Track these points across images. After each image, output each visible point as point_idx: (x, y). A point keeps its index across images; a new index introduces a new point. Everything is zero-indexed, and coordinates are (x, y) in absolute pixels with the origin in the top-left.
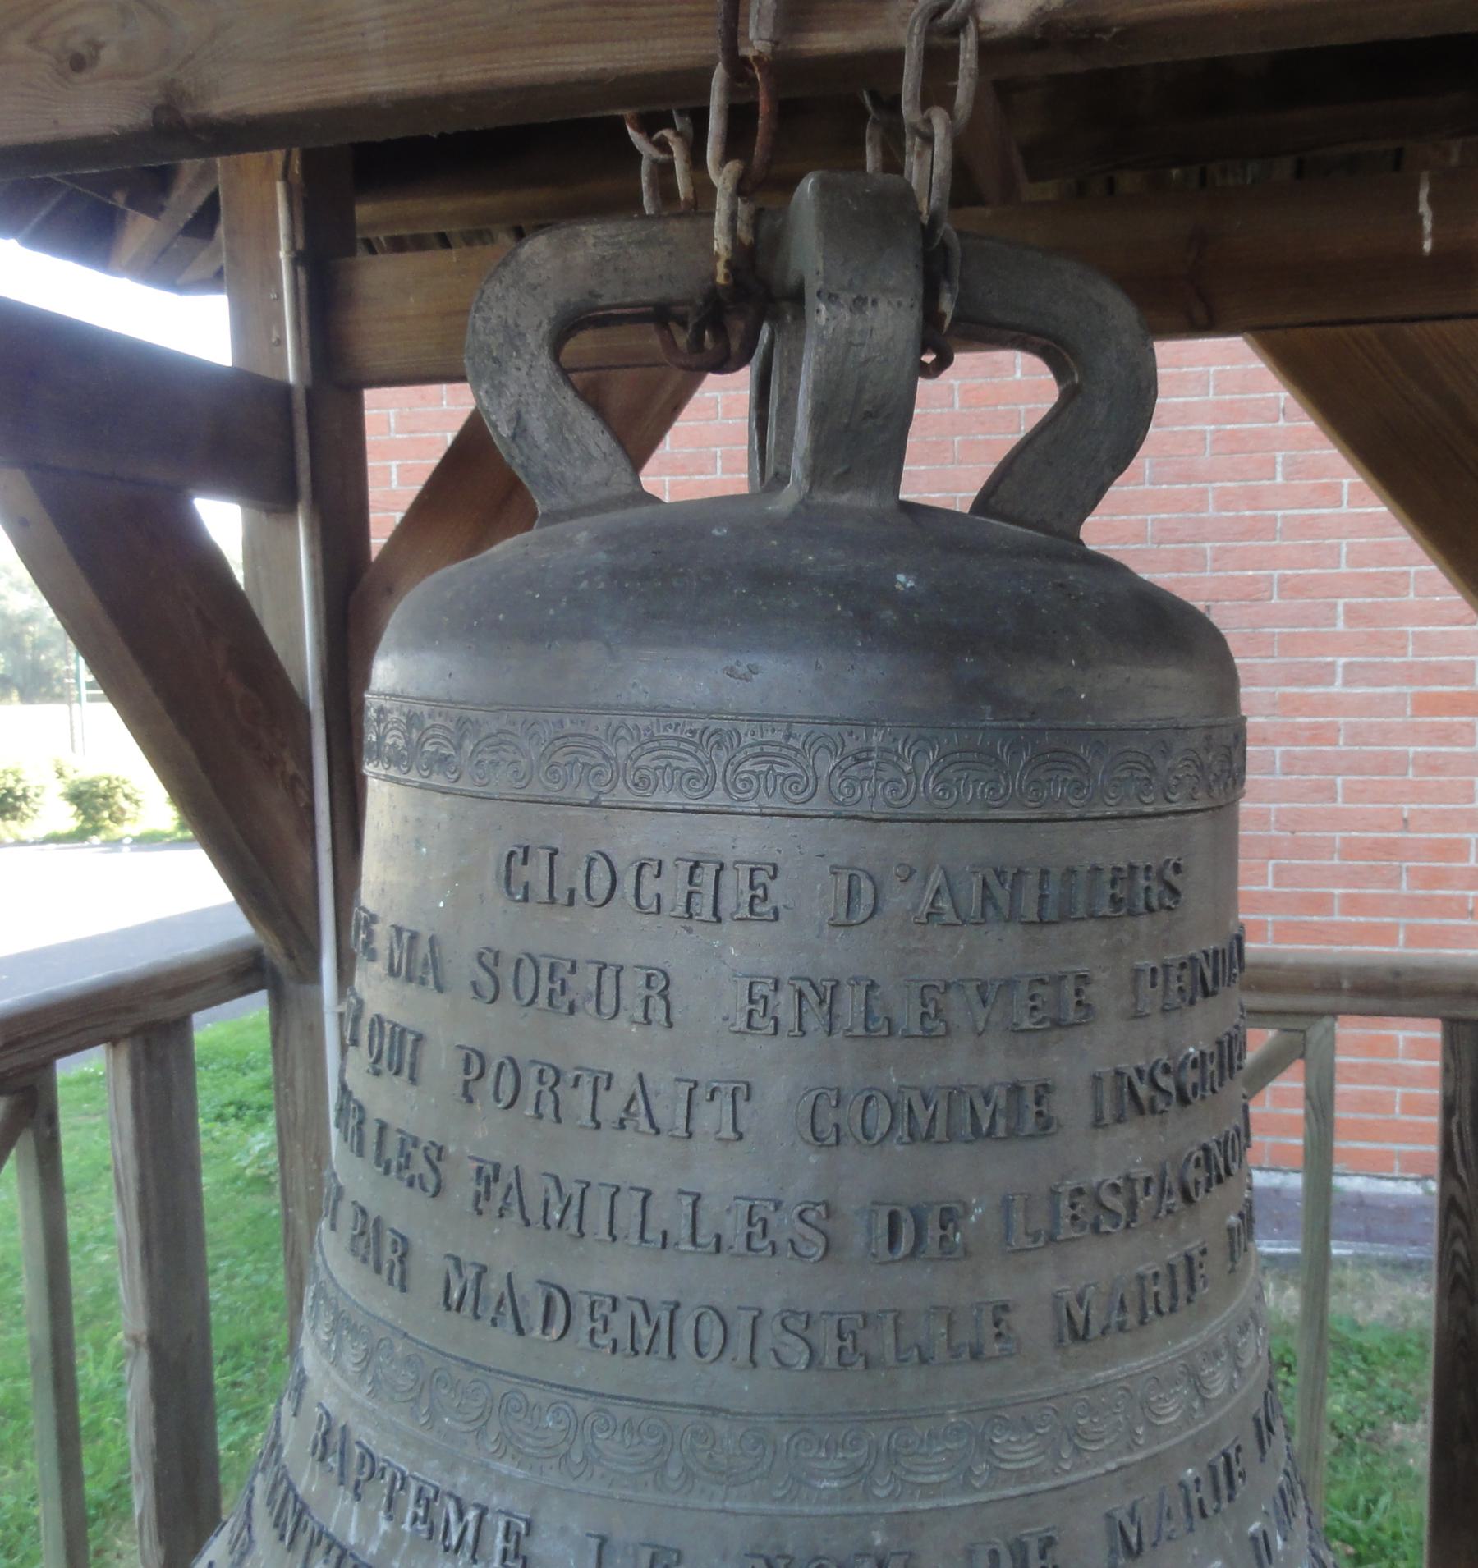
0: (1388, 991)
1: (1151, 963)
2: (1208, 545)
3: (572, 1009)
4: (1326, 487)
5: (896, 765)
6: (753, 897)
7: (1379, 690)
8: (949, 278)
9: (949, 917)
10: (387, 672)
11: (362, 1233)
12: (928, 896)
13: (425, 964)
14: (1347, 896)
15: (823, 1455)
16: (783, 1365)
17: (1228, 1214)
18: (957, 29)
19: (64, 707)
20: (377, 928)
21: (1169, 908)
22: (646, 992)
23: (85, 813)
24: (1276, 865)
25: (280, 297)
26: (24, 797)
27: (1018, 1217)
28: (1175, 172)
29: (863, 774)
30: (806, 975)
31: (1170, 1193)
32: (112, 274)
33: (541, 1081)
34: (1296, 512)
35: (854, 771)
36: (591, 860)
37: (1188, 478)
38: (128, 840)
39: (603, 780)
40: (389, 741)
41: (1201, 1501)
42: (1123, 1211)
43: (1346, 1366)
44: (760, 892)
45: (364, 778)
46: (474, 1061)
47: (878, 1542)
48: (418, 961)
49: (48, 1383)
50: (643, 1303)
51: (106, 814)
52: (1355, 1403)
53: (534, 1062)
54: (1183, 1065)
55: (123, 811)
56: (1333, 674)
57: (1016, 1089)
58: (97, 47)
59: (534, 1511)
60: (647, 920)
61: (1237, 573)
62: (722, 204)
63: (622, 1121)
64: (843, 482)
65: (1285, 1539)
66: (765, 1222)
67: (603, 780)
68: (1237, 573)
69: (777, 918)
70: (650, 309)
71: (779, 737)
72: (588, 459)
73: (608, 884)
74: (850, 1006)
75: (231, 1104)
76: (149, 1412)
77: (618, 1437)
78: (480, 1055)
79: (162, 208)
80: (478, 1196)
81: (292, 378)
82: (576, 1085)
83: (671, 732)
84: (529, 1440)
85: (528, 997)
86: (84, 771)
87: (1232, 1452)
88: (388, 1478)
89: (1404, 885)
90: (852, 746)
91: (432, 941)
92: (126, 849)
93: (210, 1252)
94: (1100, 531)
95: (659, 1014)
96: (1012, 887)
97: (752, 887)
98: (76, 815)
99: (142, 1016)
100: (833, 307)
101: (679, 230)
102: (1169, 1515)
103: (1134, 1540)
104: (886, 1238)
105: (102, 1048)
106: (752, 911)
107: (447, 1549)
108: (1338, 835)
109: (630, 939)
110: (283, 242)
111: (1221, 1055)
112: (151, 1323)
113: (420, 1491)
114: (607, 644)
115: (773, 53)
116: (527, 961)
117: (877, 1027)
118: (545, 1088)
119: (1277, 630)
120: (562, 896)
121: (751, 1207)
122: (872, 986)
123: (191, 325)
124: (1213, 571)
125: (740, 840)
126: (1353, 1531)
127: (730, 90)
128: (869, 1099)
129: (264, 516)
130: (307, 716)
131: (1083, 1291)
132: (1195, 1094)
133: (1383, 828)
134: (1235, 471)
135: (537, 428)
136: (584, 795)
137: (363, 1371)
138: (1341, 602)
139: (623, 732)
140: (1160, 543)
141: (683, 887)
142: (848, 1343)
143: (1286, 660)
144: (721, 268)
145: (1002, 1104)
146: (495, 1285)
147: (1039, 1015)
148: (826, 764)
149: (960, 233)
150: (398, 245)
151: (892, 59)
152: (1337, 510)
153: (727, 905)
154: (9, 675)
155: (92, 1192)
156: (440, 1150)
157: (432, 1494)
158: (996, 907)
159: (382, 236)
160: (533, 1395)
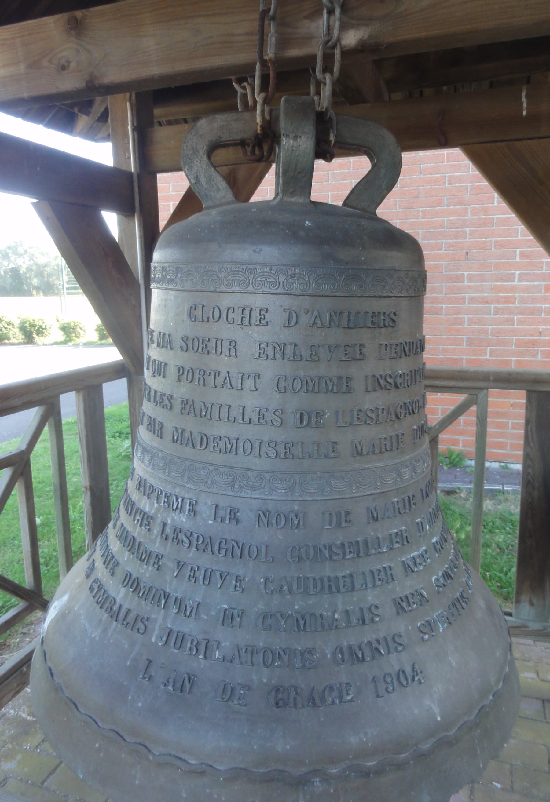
0: (507, 380)
1: (385, 343)
2: (468, 229)
3: (209, 352)
5: (303, 279)
6: (261, 318)
7: (532, 283)
8: (332, 129)
9: (320, 325)
10: (157, 256)
11: (150, 424)
12: (313, 318)
13: (167, 342)
14: (517, 360)
15: (280, 482)
16: (269, 457)
17: (413, 425)
18: (334, 47)
19: (59, 297)
20: (154, 334)
21: (392, 327)
22: (229, 347)
23: (66, 334)
24: (490, 349)
25: (129, 142)
26: (46, 329)
27: (340, 417)
28: (445, 88)
29: (293, 281)
30: (277, 341)
31: (391, 414)
32: (73, 136)
33: (200, 374)
35: (291, 280)
36: (214, 308)
37: (460, 204)
38: (81, 344)
39: (217, 284)
40: (157, 276)
41: (399, 508)
42: (375, 418)
43: (505, 526)
44: (263, 317)
45: (151, 289)
46: (181, 369)
47: (296, 509)
48: (166, 342)
49: (59, 497)
50: (229, 438)
51: (73, 335)
52: (507, 539)
53: (198, 369)
54: (397, 376)
55: (79, 333)
56: (515, 277)
57: (340, 378)
58: (69, 62)
59: (198, 498)
60: (230, 326)
61: (478, 240)
62: (259, 107)
63: (223, 385)
64: (293, 194)
65: (430, 527)
66: (264, 415)
67: (217, 284)
68: (478, 240)
69: (267, 325)
70: (238, 141)
71: (268, 270)
72: (219, 190)
73: (219, 315)
74: (289, 351)
75: (117, 432)
76: (90, 512)
77: (221, 477)
78: (183, 367)
79: (90, 112)
80: (182, 408)
81: (133, 170)
82: (210, 375)
85: (196, 349)
86: (66, 319)
87: (411, 497)
88: (157, 491)
89: (539, 357)
90: (290, 272)
91: (169, 335)
92: (81, 347)
93: (110, 479)
94: (382, 211)
95: (233, 353)
96: (339, 316)
97: (260, 315)
98: (64, 335)
99: (88, 384)
100: (288, 139)
101: (247, 115)
102: (387, 511)
103: (375, 515)
104: (299, 420)
105: (74, 392)
106: (260, 322)
107: (173, 510)
108: (514, 338)
109: (225, 331)
110: (129, 123)
111: (411, 375)
112: (90, 483)
113: (166, 494)
114: (219, 243)
115: (275, 57)
116: (196, 339)
117: (297, 358)
118: (201, 376)
120: (205, 319)
121: (260, 410)
122: (296, 345)
123: (100, 152)
124: (469, 239)
125: (258, 301)
126: (500, 578)
127: (262, 70)
128: (294, 379)
129: (124, 218)
130: (139, 285)
131: (361, 441)
132: (401, 386)
133: (532, 335)
134: (441, 192)
135: (203, 180)
136: (212, 289)
137: (150, 463)
138: (518, 250)
139: (223, 269)
140: (449, 229)
141: (240, 315)
142: (288, 451)
143: (496, 272)
144: (259, 128)
145: (336, 382)
146: (187, 434)
147: (347, 356)
148: (282, 278)
149: (336, 114)
150: (170, 123)
151: (313, 58)
153: (253, 321)
154: (39, 286)
155: (71, 459)
156: (172, 396)
157: (169, 495)
158: (334, 322)
159: (164, 120)
160: (197, 465)
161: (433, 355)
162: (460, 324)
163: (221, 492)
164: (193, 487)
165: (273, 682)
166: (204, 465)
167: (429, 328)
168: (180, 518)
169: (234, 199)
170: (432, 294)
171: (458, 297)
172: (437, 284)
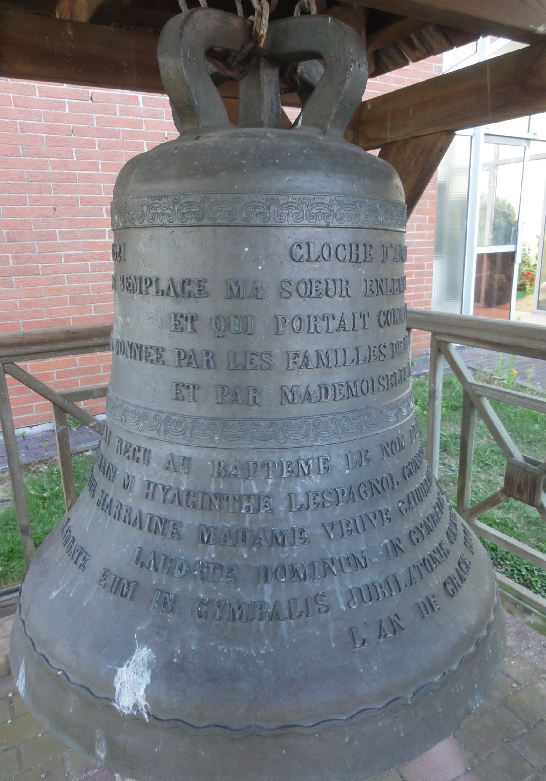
4: (93, 163)
34: (83, 172)
37: (39, 155)
56: (105, 234)
61: (64, 195)
68: (64, 195)
83: (349, 202)
84: (325, 433)
119: (82, 218)
136: (323, 223)
138: (104, 207)
140: (31, 182)
152: (98, 172)
160: (323, 419)
161: (37, 318)
162: (60, 283)
164: (324, 443)
166: (330, 417)
167: (27, 289)
169: (229, 122)
170: (24, 253)
171: (53, 255)
172: (29, 242)
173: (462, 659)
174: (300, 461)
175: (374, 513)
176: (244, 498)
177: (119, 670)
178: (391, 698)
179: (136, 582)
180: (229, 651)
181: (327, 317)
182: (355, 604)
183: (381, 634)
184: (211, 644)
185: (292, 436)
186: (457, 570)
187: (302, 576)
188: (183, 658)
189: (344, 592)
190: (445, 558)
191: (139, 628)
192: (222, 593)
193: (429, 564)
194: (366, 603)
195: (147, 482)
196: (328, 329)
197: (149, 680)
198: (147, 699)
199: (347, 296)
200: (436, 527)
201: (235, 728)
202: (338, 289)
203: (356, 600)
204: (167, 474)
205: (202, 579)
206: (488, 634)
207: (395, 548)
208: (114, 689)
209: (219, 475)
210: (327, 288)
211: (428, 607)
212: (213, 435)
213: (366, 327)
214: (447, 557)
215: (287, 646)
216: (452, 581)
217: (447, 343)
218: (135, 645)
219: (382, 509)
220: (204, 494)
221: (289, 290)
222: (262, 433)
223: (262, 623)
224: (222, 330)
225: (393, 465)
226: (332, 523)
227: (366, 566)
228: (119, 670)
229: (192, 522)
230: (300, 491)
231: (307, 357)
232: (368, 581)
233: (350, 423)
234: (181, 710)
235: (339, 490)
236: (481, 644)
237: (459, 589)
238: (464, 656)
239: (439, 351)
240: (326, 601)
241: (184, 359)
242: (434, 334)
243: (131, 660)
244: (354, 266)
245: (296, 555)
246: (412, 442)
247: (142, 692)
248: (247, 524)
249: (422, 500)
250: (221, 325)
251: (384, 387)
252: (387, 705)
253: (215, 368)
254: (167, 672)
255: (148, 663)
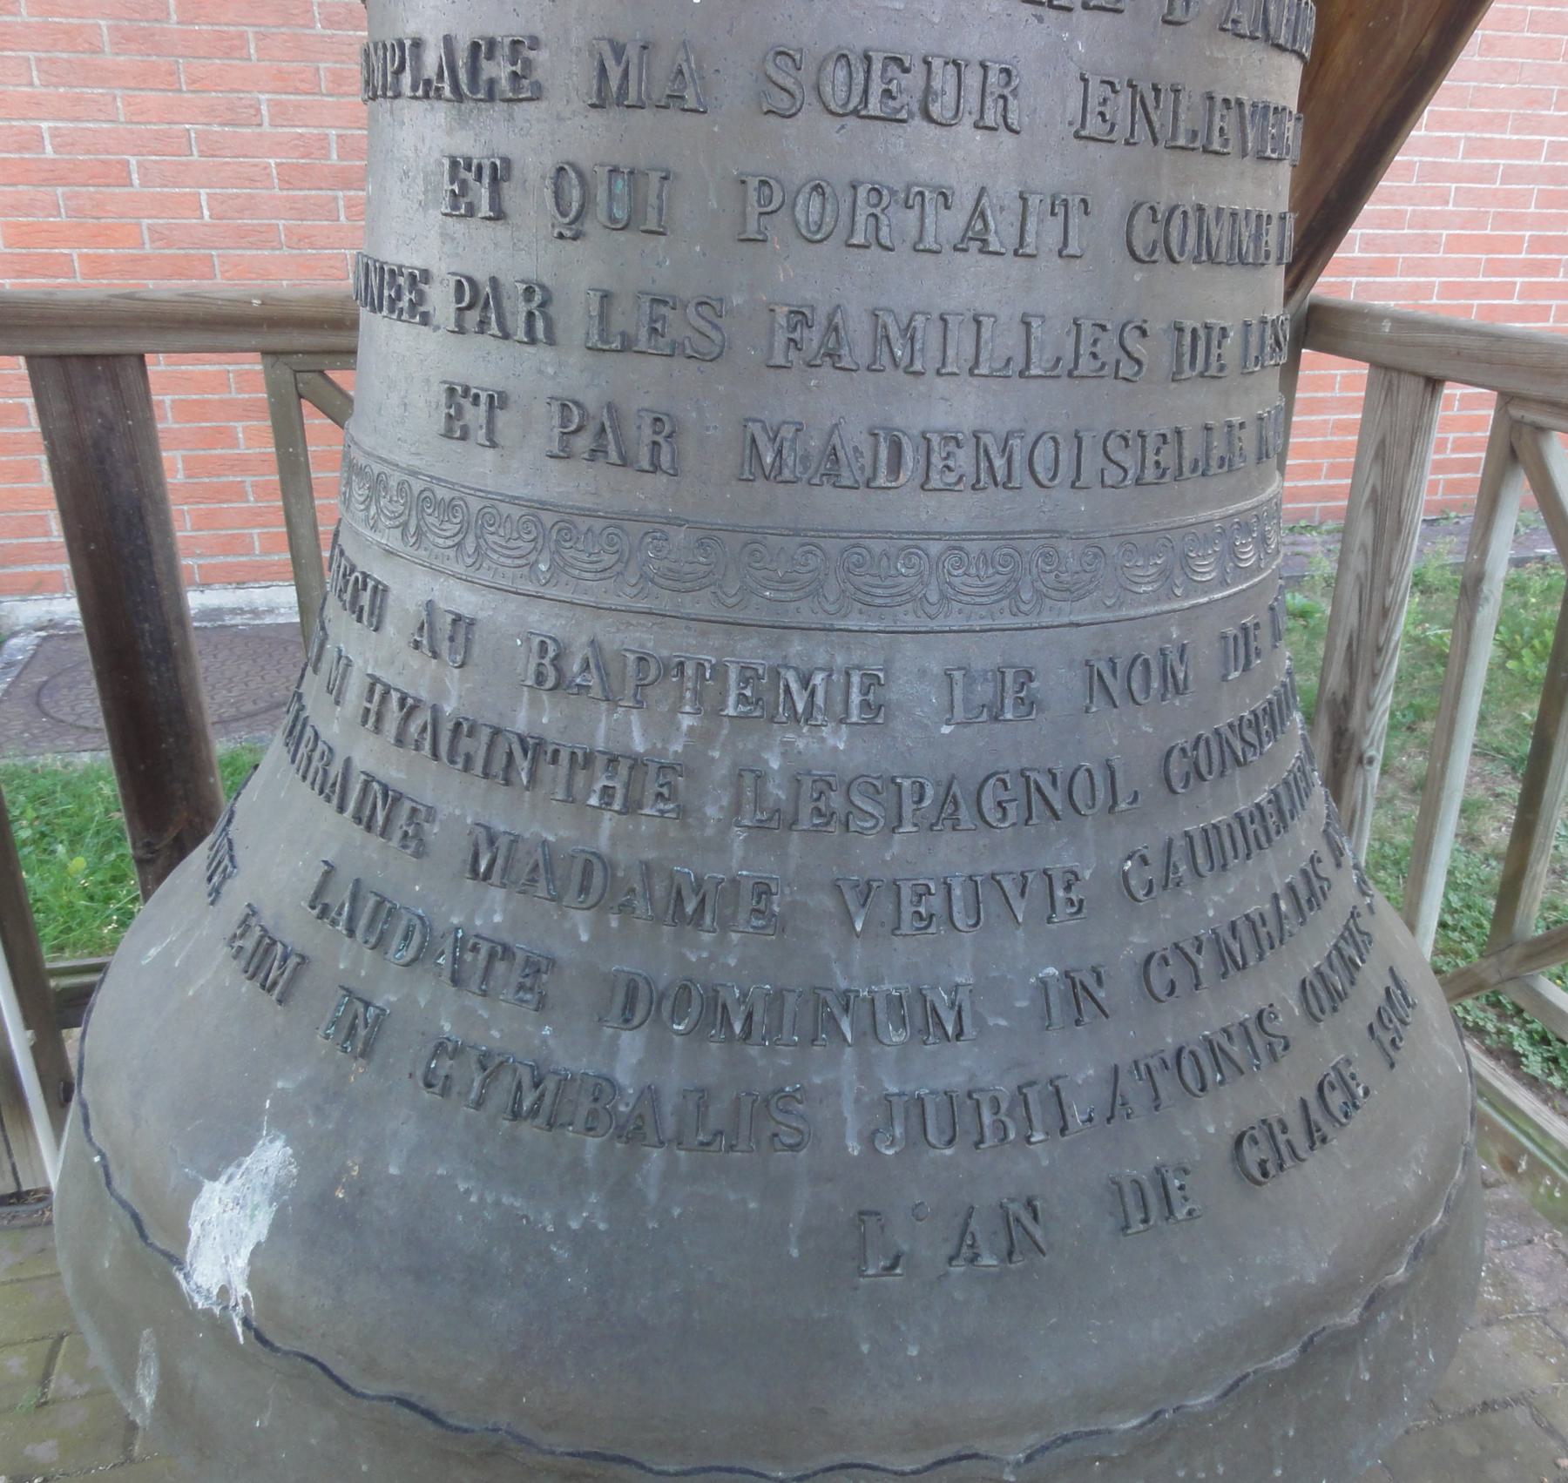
84: (880, 591)
160: (877, 546)
163: (976, 624)
164: (872, 625)
165: (1228, 1125)
168: (823, 740)
173: (1236, 1384)
174: (783, 671)
175: (1022, 874)
176: (600, 761)
177: (208, 1186)
178: (947, 1451)
179: (303, 958)
180: (481, 1198)
181: (921, 194)
182: (892, 1144)
183: (964, 1249)
184: (440, 1171)
185: (766, 588)
186: (1304, 1104)
187: (737, 1028)
188: (361, 1191)
189: (867, 1099)
190: (1265, 1060)
191: (280, 1084)
192: (501, 1031)
193: (1198, 1068)
194: (934, 1147)
195: (369, 680)
196: (921, 239)
197: (265, 1231)
198: (252, 1281)
199: (1002, 127)
200: (1261, 958)
201: (451, 1421)
202: (972, 100)
203: (898, 1131)
204: (415, 660)
205: (456, 980)
206: (1367, 1322)
207: (1080, 996)
208: (187, 1234)
209: (540, 678)
210: (928, 89)
211: (1152, 1201)
212: (532, 557)
213: (1070, 251)
214: (1274, 1057)
215: (652, 1225)
216: (1272, 1136)
217: (1541, 430)
218: (259, 1129)
219: (1056, 868)
220: (497, 732)
221: (789, 83)
222: (673, 566)
223: (592, 1142)
224: (572, 214)
225: (1129, 736)
226: (868, 883)
227: (959, 1034)
228: (208, 1186)
229: (458, 812)
230: (775, 765)
231: (836, 329)
232: (956, 1080)
233: (973, 571)
234: (323, 1336)
235: (906, 783)
236: (1325, 1351)
237: (1288, 1163)
238: (1248, 1375)
239: (1513, 456)
240: (802, 1117)
241: (470, 307)
242: (1507, 399)
243: (239, 1166)
244: (1040, 19)
245: (732, 962)
246: (1224, 678)
247: (241, 1262)
248: (603, 843)
249: (1224, 867)
250: (575, 201)
251: (1125, 471)
252: (927, 1469)
253: (551, 341)
254: (314, 1221)
255: (276, 1185)
